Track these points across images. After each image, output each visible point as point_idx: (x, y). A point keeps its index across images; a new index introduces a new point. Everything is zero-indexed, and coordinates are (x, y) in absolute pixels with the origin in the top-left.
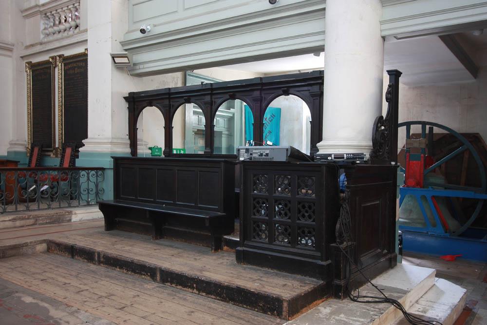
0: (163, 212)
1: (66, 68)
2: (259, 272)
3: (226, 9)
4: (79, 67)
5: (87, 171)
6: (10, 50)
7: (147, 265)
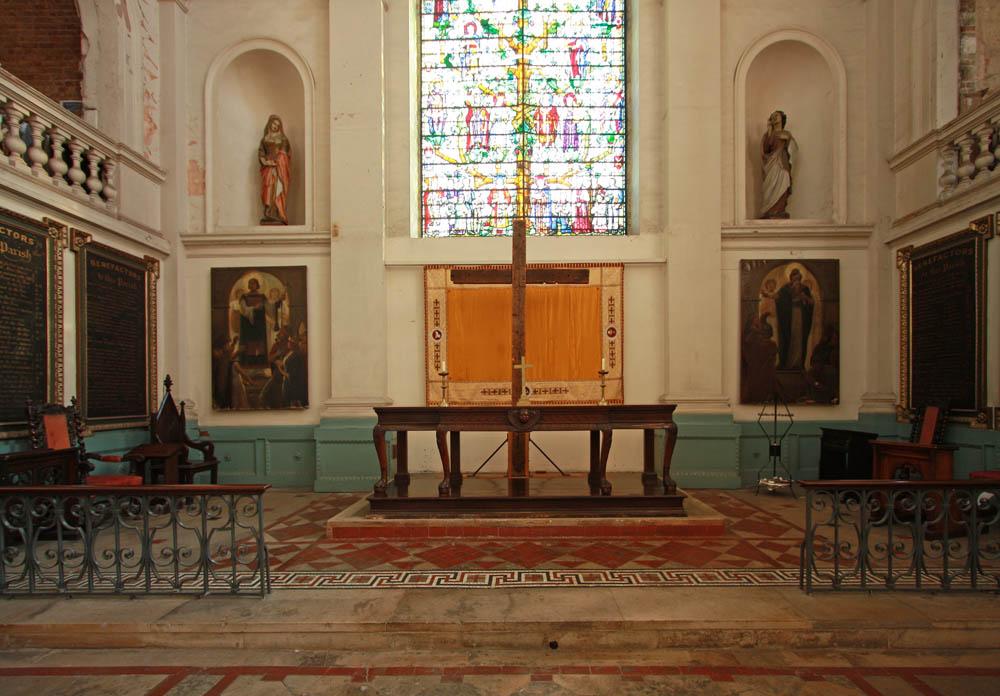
1: (916, 269)
6: (866, 236)
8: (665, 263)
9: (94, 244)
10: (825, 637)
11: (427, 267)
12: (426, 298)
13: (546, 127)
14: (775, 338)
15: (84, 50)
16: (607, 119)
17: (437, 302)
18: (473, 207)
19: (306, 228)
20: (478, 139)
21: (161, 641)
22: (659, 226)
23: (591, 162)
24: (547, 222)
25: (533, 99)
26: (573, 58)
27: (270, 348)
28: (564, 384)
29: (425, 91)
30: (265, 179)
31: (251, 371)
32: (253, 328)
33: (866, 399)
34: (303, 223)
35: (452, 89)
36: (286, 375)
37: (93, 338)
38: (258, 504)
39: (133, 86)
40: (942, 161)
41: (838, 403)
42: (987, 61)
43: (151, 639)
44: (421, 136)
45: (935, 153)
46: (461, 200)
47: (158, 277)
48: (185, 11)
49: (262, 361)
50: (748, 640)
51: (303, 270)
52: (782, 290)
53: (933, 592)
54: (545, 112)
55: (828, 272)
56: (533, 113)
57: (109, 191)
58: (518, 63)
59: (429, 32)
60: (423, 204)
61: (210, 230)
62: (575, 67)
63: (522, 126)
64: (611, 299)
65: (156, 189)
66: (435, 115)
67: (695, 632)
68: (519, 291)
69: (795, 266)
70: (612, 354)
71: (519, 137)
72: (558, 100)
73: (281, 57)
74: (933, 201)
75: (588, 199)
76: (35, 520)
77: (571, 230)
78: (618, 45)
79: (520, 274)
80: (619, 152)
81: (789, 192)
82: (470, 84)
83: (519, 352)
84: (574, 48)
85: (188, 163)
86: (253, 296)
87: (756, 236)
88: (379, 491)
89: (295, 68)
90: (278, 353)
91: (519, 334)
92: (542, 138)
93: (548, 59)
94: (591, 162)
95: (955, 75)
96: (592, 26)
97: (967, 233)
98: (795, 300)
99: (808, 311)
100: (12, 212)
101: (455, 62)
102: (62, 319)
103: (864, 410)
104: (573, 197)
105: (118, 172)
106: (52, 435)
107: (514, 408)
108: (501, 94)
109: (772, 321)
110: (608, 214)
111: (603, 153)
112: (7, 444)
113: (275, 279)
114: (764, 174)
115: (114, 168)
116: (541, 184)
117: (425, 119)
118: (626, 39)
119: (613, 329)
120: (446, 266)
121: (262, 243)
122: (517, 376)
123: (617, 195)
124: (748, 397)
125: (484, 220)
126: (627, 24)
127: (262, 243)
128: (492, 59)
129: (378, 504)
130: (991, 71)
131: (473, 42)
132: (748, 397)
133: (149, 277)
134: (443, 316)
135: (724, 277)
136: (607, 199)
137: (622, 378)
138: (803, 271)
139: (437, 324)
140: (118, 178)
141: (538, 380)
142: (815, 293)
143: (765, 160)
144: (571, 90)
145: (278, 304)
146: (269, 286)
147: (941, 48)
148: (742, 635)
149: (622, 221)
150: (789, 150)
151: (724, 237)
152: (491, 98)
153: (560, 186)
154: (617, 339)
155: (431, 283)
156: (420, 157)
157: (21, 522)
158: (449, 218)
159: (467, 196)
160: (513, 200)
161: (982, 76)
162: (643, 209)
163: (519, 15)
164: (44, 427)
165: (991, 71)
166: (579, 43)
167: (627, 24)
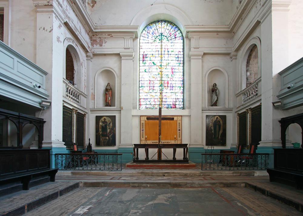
4: (69, 113)
6: (232, 110)
8: (190, 116)
9: (78, 112)
10: (202, 174)
11: (141, 116)
12: (141, 122)
13: (166, 85)
14: (213, 132)
15: (74, 73)
16: (180, 84)
17: (143, 123)
18: (150, 102)
19: (115, 107)
20: (152, 88)
21: (109, 175)
22: (189, 108)
23: (176, 93)
24: (166, 106)
25: (163, 79)
26: (172, 70)
27: (108, 133)
28: (169, 141)
29: (140, 77)
30: (107, 97)
31: (104, 138)
32: (104, 128)
33: (232, 145)
34: (115, 106)
35: (145, 77)
36: (111, 139)
38: (121, 157)
39: (83, 78)
40: (243, 97)
41: (226, 145)
42: (255, 75)
43: (108, 174)
44: (139, 87)
45: (242, 95)
46: (148, 101)
48: (91, 61)
49: (106, 136)
50: (191, 175)
51: (115, 116)
52: (214, 122)
53: (220, 170)
54: (166, 82)
55: (224, 118)
56: (163, 82)
57: (79, 101)
58: (160, 71)
59: (141, 64)
60: (139, 102)
61: (95, 108)
62: (173, 72)
63: (161, 85)
64: (179, 123)
65: (85, 99)
66: (142, 82)
67: (184, 174)
68: (160, 122)
69: (218, 116)
70: (179, 135)
71: (160, 87)
72: (169, 79)
73: (111, 71)
74: (241, 105)
75: (175, 101)
77: (172, 108)
78: (182, 68)
79: (160, 118)
80: (182, 91)
81: (217, 100)
82: (150, 76)
83: (160, 134)
84: (172, 68)
85: (91, 93)
86: (104, 122)
87: (209, 110)
88: (134, 159)
89: (114, 73)
90: (110, 134)
91: (160, 130)
92: (165, 88)
93: (167, 70)
94: (176, 93)
95: (246, 80)
96: (176, 64)
97: (245, 112)
98: (217, 124)
99: (220, 126)
101: (147, 71)
103: (231, 147)
104: (172, 100)
105: (80, 97)
107: (159, 144)
108: (157, 78)
109: (212, 128)
110: (179, 104)
111: (179, 91)
113: (109, 118)
114: (212, 96)
116: (165, 97)
117: (140, 83)
118: (183, 66)
119: (179, 129)
120: (145, 116)
121: (107, 110)
122: (159, 139)
123: (182, 100)
124: (207, 144)
125: (153, 105)
126: (183, 63)
127: (107, 110)
128: (155, 70)
129: (134, 161)
130: (255, 77)
131: (151, 67)
132: (207, 144)
134: (144, 126)
135: (202, 119)
136: (179, 101)
137: (181, 140)
138: (219, 118)
139: (143, 128)
140: (80, 99)
141: (164, 140)
142: (221, 122)
143: (212, 94)
144: (172, 77)
145: (110, 123)
146: (108, 120)
147: (243, 74)
148: (190, 174)
149: (182, 106)
150: (217, 92)
151: (202, 110)
152: (154, 79)
153: (169, 98)
154: (180, 131)
155: (142, 119)
156: (139, 91)
158: (145, 105)
159: (149, 100)
160: (159, 101)
161: (254, 78)
162: (186, 104)
163: (161, 61)
165: (255, 77)
166: (174, 67)
167: (183, 63)
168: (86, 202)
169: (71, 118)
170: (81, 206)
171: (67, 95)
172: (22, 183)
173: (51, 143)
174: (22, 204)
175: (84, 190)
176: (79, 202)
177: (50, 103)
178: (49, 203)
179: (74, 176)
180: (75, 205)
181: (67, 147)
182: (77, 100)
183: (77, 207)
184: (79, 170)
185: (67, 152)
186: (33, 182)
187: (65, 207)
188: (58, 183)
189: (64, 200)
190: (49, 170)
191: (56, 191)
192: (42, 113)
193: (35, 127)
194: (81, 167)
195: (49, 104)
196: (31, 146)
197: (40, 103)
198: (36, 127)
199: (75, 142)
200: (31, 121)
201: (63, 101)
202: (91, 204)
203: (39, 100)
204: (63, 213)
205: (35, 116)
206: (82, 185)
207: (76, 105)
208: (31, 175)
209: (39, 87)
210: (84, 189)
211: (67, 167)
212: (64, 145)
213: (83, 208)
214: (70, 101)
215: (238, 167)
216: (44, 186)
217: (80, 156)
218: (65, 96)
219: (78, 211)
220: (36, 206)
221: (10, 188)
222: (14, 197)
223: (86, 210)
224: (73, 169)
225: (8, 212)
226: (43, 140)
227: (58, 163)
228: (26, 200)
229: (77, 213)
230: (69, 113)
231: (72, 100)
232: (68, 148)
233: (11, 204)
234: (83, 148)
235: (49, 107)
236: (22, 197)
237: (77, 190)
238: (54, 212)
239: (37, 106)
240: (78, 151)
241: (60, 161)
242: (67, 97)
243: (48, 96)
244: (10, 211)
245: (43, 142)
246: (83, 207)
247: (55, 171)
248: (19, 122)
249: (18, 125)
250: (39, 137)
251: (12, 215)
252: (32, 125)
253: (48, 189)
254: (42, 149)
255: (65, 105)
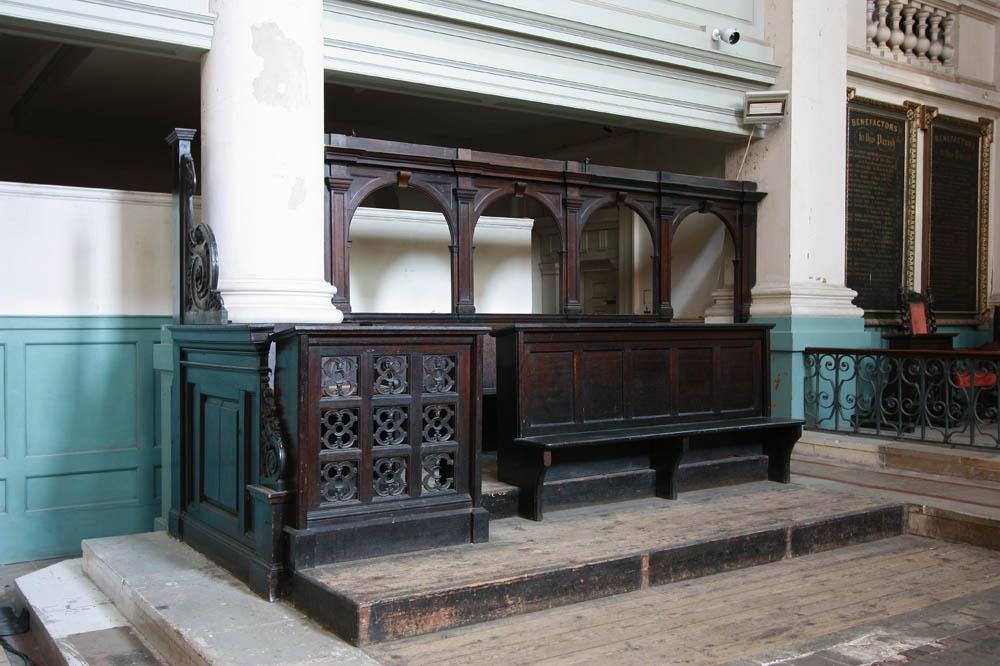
0: (757, 429)
2: (432, 556)
3: (675, 23)
4: (887, 134)
5: (854, 356)
7: (292, 608)
9: (940, 117)
37: (934, 218)
47: (991, 141)
57: (948, 52)
76: (928, 379)
100: (877, 102)
102: (914, 204)
105: (957, 27)
106: (916, 323)
112: (876, 331)
115: (952, 22)
133: (983, 141)
140: (956, 37)
157: (917, 379)
164: (910, 315)
168: (913, 616)
169: (897, 157)
170: (876, 624)
171: (876, 41)
172: (651, 468)
173: (786, 295)
174: (632, 547)
175: (931, 552)
176: (874, 606)
177: (783, 101)
178: (740, 572)
179: (892, 471)
180: (845, 614)
181: (866, 316)
182: (937, 49)
183: (852, 623)
184: (926, 444)
185: (868, 339)
186: (693, 468)
187: (800, 607)
188: (801, 493)
189: (806, 576)
190: (764, 421)
191: (778, 526)
192: (750, 154)
193: (723, 228)
194: (936, 423)
195: (776, 108)
196: (707, 312)
197: (740, 114)
198: (729, 227)
199: (918, 289)
200: (703, 201)
201: (850, 73)
202: (934, 630)
203: (733, 98)
204: (781, 631)
205: (723, 176)
206: (922, 525)
207: (924, 83)
208: (686, 435)
209: (735, 38)
210: (926, 546)
211: (864, 422)
212: (854, 302)
213: (880, 639)
214: (893, 65)
215: (950, 431)
216: (736, 495)
217: (929, 365)
218: (861, 43)
219: (852, 643)
220: (683, 570)
221: (613, 479)
222: (620, 517)
223: (894, 655)
224: (895, 434)
225: (584, 564)
226: (752, 282)
227: (818, 395)
228: (650, 537)
229: (846, 652)
230: (887, 134)
231: (902, 58)
232: (875, 321)
233: (600, 539)
234: (970, 321)
235: (779, 122)
236: (644, 523)
237: (891, 543)
238: (746, 616)
239: (729, 125)
240: (929, 339)
241: (826, 387)
242: (875, 51)
243: (773, 70)
244: (592, 561)
245: (754, 291)
246: (881, 632)
247: (792, 432)
248: (659, 212)
249: (654, 222)
250: (735, 269)
251: (597, 578)
252: (707, 216)
253: (745, 509)
254: (750, 322)
255: (865, 92)
